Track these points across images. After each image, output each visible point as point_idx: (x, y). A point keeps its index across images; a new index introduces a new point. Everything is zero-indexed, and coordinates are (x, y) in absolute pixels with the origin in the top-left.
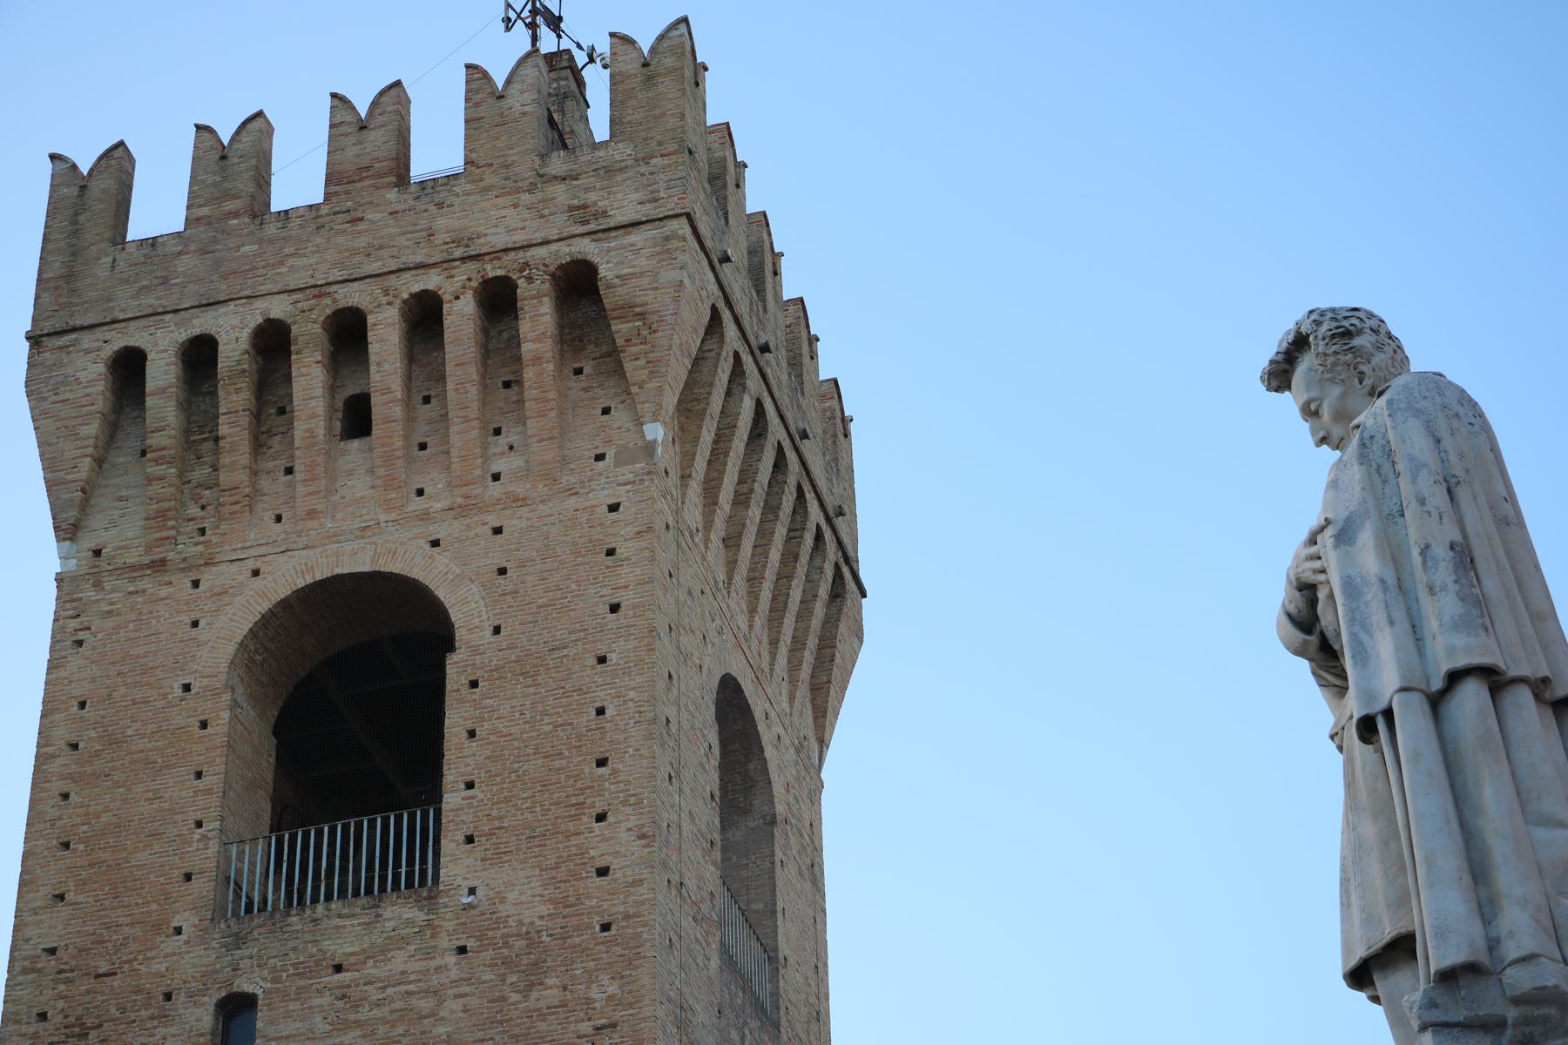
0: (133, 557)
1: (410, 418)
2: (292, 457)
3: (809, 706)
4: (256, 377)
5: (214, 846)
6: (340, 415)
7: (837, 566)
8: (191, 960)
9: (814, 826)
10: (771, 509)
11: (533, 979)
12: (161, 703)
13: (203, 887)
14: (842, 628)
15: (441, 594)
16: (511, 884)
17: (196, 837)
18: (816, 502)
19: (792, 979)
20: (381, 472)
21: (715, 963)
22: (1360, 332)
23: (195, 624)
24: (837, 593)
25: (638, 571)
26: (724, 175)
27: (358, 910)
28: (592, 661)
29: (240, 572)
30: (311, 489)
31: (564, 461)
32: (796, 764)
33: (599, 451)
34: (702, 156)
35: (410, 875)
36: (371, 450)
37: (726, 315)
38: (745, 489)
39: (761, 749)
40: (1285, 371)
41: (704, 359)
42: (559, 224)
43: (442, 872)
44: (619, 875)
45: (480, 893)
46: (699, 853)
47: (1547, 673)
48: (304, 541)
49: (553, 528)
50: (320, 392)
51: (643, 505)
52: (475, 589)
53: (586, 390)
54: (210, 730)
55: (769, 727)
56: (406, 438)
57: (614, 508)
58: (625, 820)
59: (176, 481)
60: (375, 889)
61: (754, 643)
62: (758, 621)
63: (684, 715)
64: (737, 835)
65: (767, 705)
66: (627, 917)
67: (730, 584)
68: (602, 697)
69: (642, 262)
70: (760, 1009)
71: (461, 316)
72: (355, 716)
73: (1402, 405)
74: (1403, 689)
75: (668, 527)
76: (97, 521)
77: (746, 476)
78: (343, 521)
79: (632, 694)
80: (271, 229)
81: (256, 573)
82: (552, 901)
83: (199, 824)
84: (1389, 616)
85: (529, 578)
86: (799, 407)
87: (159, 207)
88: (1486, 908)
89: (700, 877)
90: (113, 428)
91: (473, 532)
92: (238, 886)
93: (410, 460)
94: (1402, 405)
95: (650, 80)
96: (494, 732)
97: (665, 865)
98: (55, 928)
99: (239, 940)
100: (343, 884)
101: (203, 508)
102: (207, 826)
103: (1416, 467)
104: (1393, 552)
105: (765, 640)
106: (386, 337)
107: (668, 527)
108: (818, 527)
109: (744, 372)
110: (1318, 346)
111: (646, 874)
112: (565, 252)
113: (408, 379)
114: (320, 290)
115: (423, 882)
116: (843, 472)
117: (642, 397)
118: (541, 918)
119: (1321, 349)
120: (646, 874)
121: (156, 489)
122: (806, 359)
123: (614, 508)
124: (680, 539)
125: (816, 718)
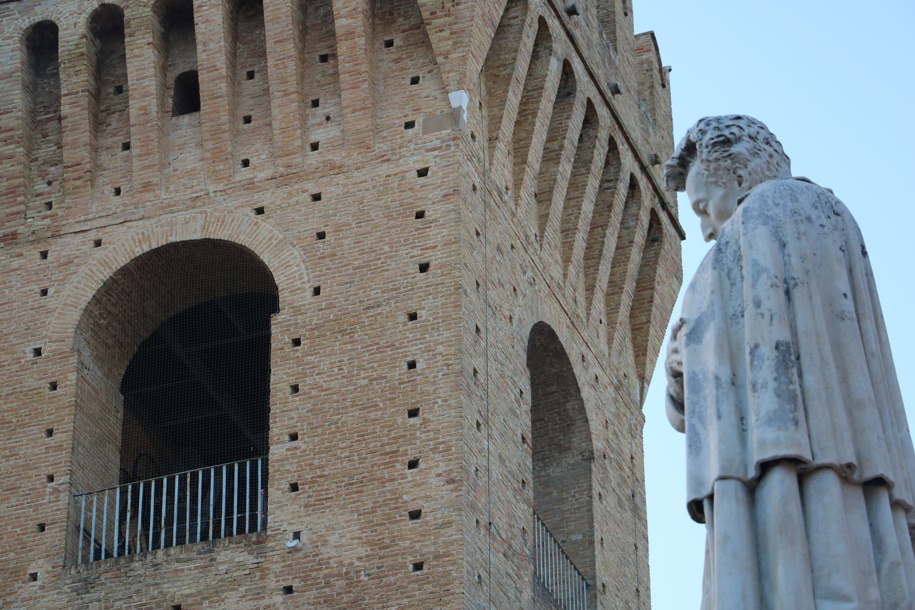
1: (235, 92)
2: (128, 133)
3: (629, 345)
4: (94, 59)
5: (64, 498)
6: (172, 92)
7: (653, 212)
10: (582, 163)
12: (15, 367)
13: (55, 536)
14: (660, 270)
15: (266, 258)
16: (331, 528)
17: (48, 490)
18: (630, 154)
20: (209, 145)
21: (527, 594)
22: (739, 139)
23: (44, 292)
25: (445, 232)
27: (194, 555)
28: (404, 318)
29: (83, 243)
30: (147, 162)
31: (376, 130)
32: (615, 401)
33: (409, 119)
35: (241, 520)
36: (200, 124)
38: (555, 145)
39: (578, 390)
40: (681, 174)
41: (510, 25)
43: (269, 518)
44: (430, 518)
45: (304, 537)
46: (509, 493)
47: (852, 459)
48: (141, 212)
49: (367, 194)
50: (151, 71)
51: (449, 170)
52: (296, 253)
53: (396, 61)
54: (59, 391)
55: (586, 369)
56: (232, 113)
57: (423, 173)
58: (435, 466)
59: (23, 159)
60: (211, 536)
61: (569, 292)
62: (572, 270)
63: (493, 366)
64: (555, 471)
65: (584, 349)
66: (437, 557)
67: (542, 237)
68: (413, 351)
73: (755, 213)
74: (722, 478)
75: (474, 188)
79: (441, 348)
81: (98, 243)
82: (368, 543)
83: (51, 478)
84: (718, 411)
85: (346, 242)
86: (611, 62)
89: (511, 516)
91: (295, 199)
92: (87, 533)
93: (236, 133)
94: (755, 213)
96: (316, 386)
97: (473, 507)
99: (88, 585)
100: (181, 530)
101: (49, 183)
102: (59, 480)
103: (758, 271)
104: (730, 350)
105: (581, 286)
107: (474, 188)
108: (632, 177)
109: (550, 36)
110: (703, 153)
111: (454, 516)
113: (233, 56)
115: (253, 528)
116: (660, 120)
117: (447, 67)
118: (359, 559)
119: (704, 156)
120: (454, 516)
122: (620, 17)
123: (423, 173)
124: (488, 198)
125: (637, 356)
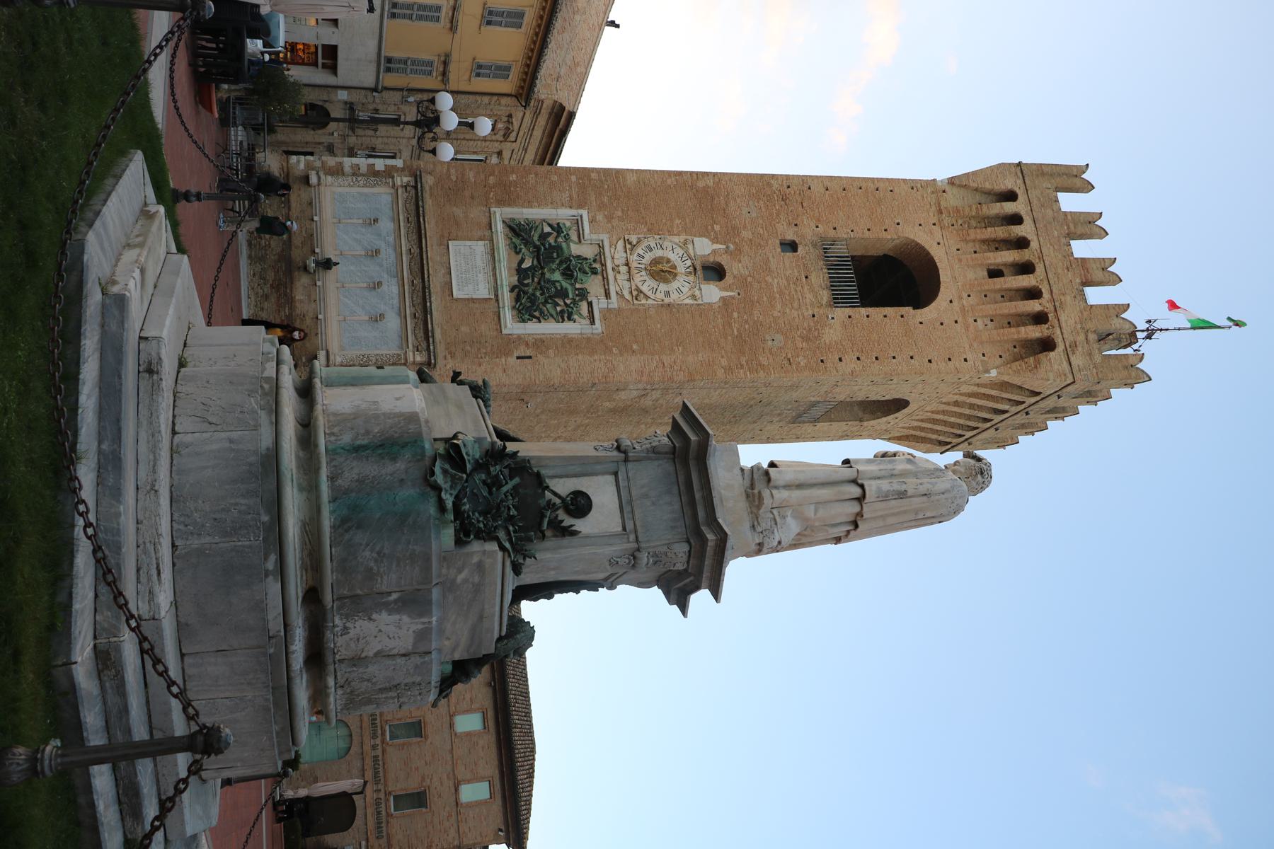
0: (943, 203)
1: (996, 291)
8: (808, 232)
9: (860, 437)
10: (969, 417)
11: (806, 339)
13: (832, 233)
19: (809, 428)
24: (942, 443)
26: (1092, 396)
31: (982, 343)
34: (1097, 387)
37: (1038, 398)
42: (1069, 338)
58: (858, 366)
60: (833, 288)
64: (856, 408)
68: (899, 358)
69: (1056, 367)
70: (799, 416)
71: (1034, 306)
72: (892, 279)
76: (955, 190)
77: (980, 408)
78: (958, 270)
80: (1063, 240)
87: (1069, 202)
88: (788, 487)
90: (988, 193)
95: (1126, 367)
98: (817, 188)
99: (815, 246)
103: (934, 484)
104: (904, 474)
106: (1026, 281)
110: (978, 464)
112: (1059, 341)
113: (1010, 290)
114: (1041, 258)
121: (967, 209)
